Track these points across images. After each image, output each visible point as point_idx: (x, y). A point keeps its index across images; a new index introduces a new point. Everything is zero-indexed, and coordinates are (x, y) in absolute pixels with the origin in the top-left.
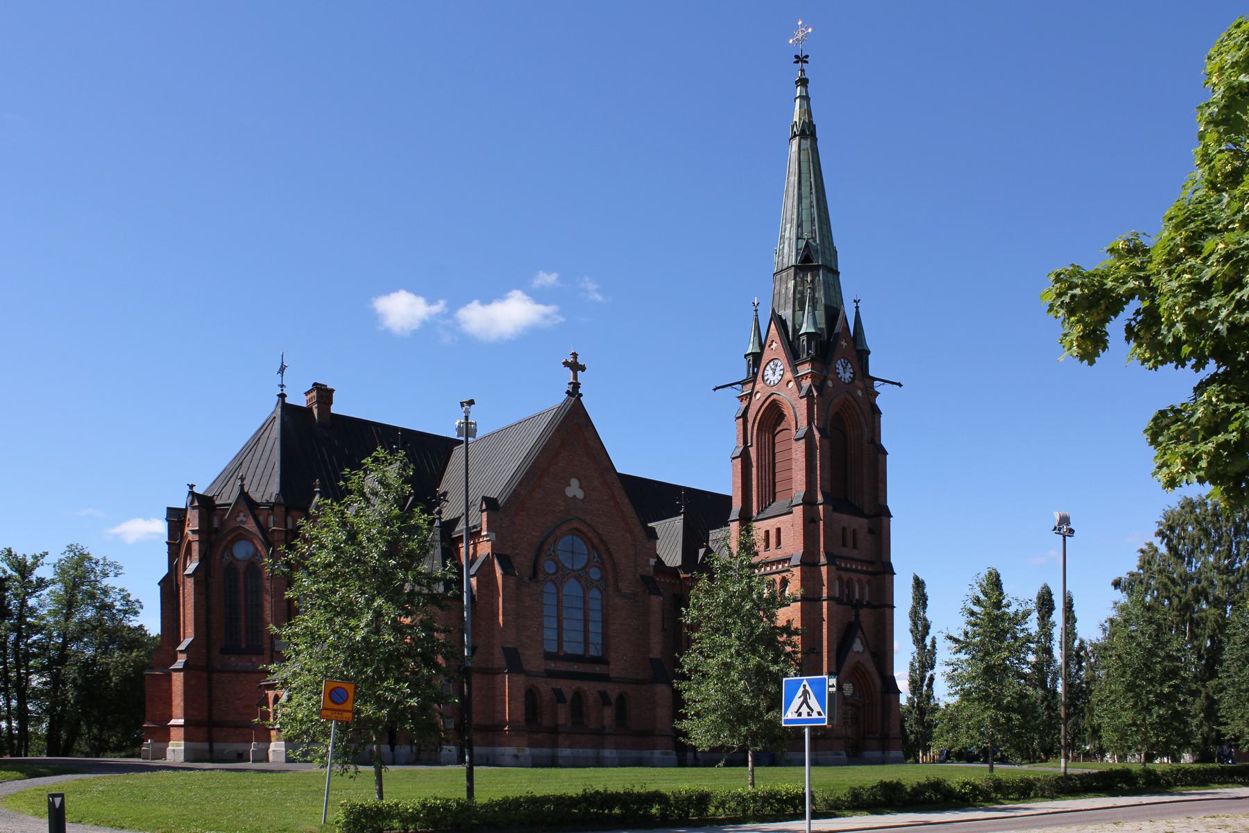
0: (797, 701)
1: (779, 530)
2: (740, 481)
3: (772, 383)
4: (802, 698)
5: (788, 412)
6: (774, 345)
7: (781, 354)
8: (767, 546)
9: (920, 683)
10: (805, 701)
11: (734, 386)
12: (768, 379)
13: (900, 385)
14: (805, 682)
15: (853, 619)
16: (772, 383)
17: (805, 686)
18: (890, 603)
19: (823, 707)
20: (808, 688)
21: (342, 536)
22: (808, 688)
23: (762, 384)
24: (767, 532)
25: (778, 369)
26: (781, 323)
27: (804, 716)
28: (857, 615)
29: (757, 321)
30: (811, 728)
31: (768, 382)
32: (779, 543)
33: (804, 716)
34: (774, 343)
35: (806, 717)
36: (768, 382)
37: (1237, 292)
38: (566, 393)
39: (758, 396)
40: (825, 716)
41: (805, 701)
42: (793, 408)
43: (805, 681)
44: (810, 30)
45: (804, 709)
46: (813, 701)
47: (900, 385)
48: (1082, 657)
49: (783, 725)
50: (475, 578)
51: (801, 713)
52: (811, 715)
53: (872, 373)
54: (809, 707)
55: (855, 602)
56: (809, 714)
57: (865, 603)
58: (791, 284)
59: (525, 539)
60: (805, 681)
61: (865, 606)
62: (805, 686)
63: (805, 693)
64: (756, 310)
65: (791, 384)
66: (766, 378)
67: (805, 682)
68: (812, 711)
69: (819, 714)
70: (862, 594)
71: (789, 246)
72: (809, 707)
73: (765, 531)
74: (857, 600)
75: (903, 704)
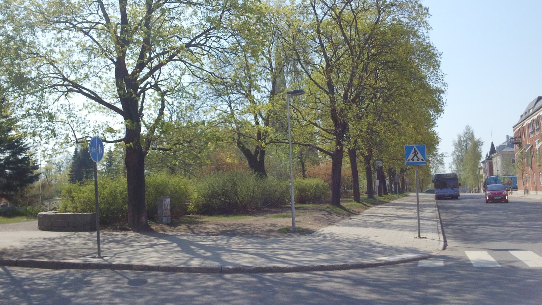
9: (374, 189)
10: (416, 155)
14: (415, 147)
17: (415, 149)
21: (257, 78)
22: (416, 149)
33: (416, 161)
35: (417, 161)
37: (160, 276)
41: (416, 155)
45: (415, 158)
50: (479, 167)
54: (417, 157)
56: (418, 160)
59: (265, 28)
62: (415, 149)
63: (415, 152)
69: (422, 160)
72: (417, 157)
75: (74, 79)
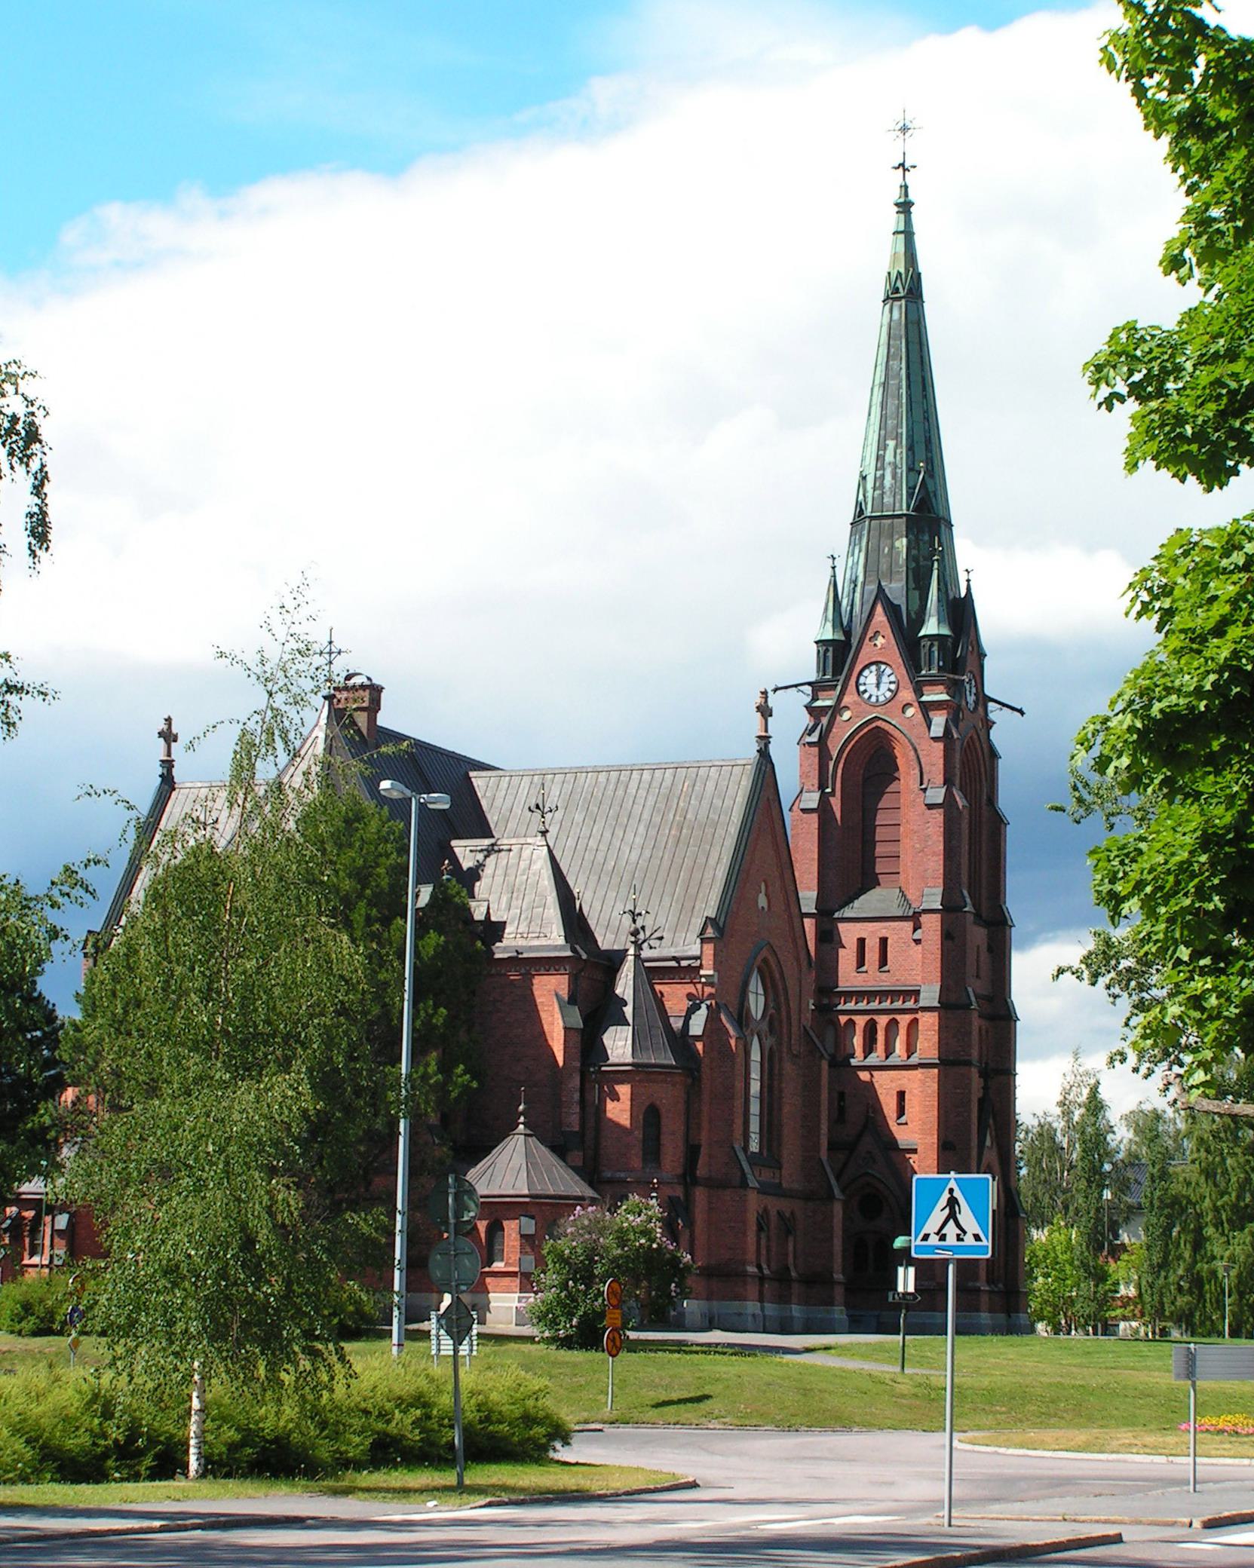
1: (884, 941)
2: (816, 850)
4: (947, 1211)
5: (903, 756)
6: (880, 641)
7: (895, 656)
8: (861, 962)
10: (952, 1216)
11: (800, 688)
12: (865, 691)
13: (1022, 712)
14: (952, 1184)
17: (951, 1191)
18: (851, 1052)
19: (982, 1225)
22: (957, 1194)
23: (856, 697)
24: (861, 942)
25: (885, 679)
26: (892, 611)
27: (951, 1240)
30: (960, 1263)
31: (866, 696)
32: (883, 961)
34: (880, 638)
35: (955, 1242)
36: (866, 696)
39: (847, 715)
40: (987, 1242)
41: (952, 1216)
42: (916, 750)
43: (952, 1181)
45: (951, 1230)
47: (1022, 712)
48: (1104, 1176)
49: (913, 1255)
51: (945, 1235)
52: (962, 1240)
53: (989, 691)
56: (959, 1239)
58: (902, 543)
60: (952, 1181)
62: (951, 1191)
63: (952, 1202)
64: (834, 568)
65: (910, 712)
66: (862, 688)
67: (952, 1184)
68: (965, 1232)
69: (977, 1237)
71: (894, 477)
73: (858, 939)
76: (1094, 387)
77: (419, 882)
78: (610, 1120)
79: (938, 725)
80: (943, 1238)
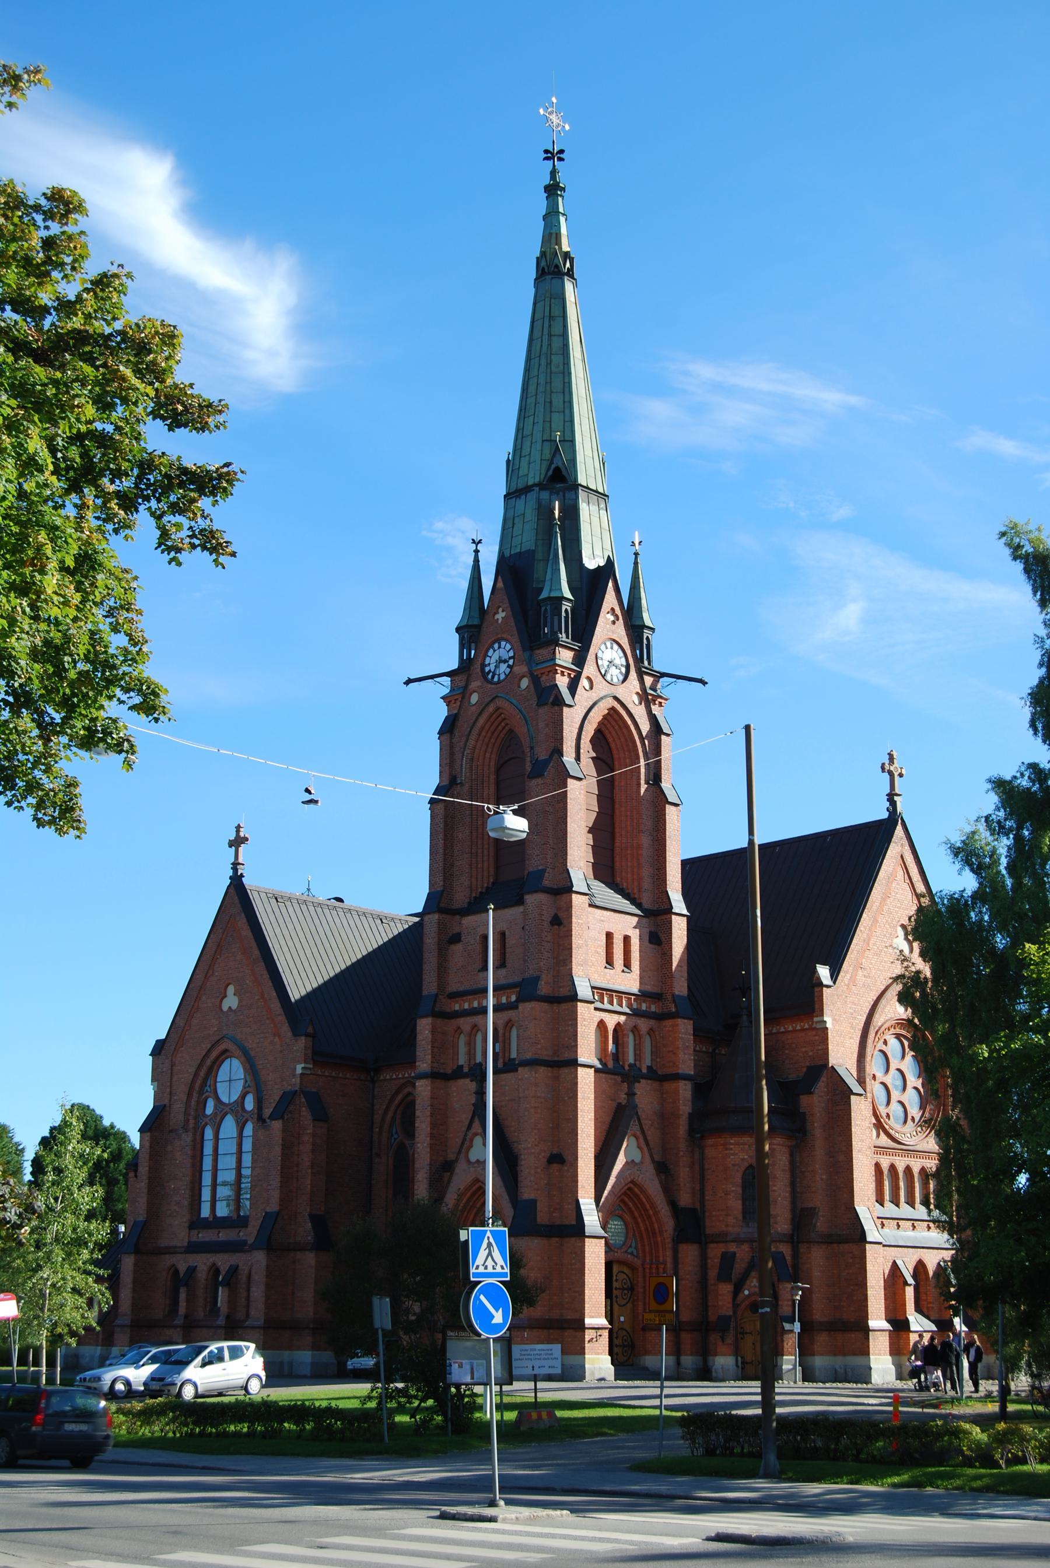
0: (483, 1253)
3: (496, 679)
10: (490, 1254)
13: (704, 683)
14: (488, 1234)
15: (623, 1098)
16: (496, 679)
17: (488, 1238)
20: (492, 1240)
28: (631, 1094)
29: (476, 561)
33: (490, 1270)
38: (230, 846)
40: (507, 1270)
41: (490, 1254)
43: (488, 1233)
44: (554, 100)
45: (490, 1263)
46: (496, 1254)
47: (704, 683)
49: (472, 1279)
55: (627, 1068)
56: (494, 1269)
57: (644, 1071)
60: (488, 1233)
61: (644, 1077)
62: (488, 1238)
63: (489, 1245)
67: (488, 1234)
68: (496, 1264)
69: (502, 1267)
70: (638, 1055)
74: (630, 1065)
76: (242, 834)
77: (467, 1241)
78: (693, 1109)
79: (826, 977)
80: (486, 1268)
